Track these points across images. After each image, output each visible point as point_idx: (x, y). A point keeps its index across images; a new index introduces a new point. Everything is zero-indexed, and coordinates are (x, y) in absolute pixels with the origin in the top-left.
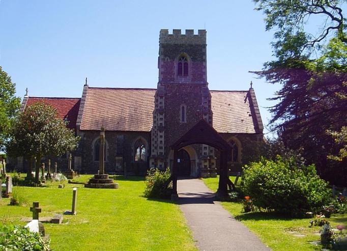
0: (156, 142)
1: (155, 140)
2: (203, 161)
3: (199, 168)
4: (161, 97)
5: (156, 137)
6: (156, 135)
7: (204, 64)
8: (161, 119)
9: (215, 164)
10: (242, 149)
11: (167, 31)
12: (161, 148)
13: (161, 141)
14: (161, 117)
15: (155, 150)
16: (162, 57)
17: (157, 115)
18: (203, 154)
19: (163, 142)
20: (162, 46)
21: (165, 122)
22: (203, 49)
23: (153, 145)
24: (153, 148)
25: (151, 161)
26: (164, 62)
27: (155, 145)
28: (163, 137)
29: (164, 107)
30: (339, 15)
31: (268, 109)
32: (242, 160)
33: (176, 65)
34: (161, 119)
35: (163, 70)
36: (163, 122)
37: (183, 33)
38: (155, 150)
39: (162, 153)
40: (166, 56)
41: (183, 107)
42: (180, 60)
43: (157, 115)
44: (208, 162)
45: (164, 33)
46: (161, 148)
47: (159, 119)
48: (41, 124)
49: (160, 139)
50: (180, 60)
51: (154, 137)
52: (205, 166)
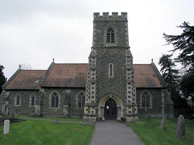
1: (89, 91)
2: (127, 108)
4: (94, 57)
8: (93, 74)
9: (137, 109)
14: (93, 72)
20: (95, 22)
21: (97, 77)
22: (125, 24)
23: (87, 95)
28: (95, 88)
33: (105, 35)
34: (93, 74)
35: (95, 39)
36: (95, 76)
37: (110, 14)
39: (94, 101)
40: (97, 29)
41: (111, 65)
42: (108, 32)
45: (96, 14)
46: (93, 97)
47: (91, 75)
50: (108, 32)
51: (88, 89)
52: (130, 112)
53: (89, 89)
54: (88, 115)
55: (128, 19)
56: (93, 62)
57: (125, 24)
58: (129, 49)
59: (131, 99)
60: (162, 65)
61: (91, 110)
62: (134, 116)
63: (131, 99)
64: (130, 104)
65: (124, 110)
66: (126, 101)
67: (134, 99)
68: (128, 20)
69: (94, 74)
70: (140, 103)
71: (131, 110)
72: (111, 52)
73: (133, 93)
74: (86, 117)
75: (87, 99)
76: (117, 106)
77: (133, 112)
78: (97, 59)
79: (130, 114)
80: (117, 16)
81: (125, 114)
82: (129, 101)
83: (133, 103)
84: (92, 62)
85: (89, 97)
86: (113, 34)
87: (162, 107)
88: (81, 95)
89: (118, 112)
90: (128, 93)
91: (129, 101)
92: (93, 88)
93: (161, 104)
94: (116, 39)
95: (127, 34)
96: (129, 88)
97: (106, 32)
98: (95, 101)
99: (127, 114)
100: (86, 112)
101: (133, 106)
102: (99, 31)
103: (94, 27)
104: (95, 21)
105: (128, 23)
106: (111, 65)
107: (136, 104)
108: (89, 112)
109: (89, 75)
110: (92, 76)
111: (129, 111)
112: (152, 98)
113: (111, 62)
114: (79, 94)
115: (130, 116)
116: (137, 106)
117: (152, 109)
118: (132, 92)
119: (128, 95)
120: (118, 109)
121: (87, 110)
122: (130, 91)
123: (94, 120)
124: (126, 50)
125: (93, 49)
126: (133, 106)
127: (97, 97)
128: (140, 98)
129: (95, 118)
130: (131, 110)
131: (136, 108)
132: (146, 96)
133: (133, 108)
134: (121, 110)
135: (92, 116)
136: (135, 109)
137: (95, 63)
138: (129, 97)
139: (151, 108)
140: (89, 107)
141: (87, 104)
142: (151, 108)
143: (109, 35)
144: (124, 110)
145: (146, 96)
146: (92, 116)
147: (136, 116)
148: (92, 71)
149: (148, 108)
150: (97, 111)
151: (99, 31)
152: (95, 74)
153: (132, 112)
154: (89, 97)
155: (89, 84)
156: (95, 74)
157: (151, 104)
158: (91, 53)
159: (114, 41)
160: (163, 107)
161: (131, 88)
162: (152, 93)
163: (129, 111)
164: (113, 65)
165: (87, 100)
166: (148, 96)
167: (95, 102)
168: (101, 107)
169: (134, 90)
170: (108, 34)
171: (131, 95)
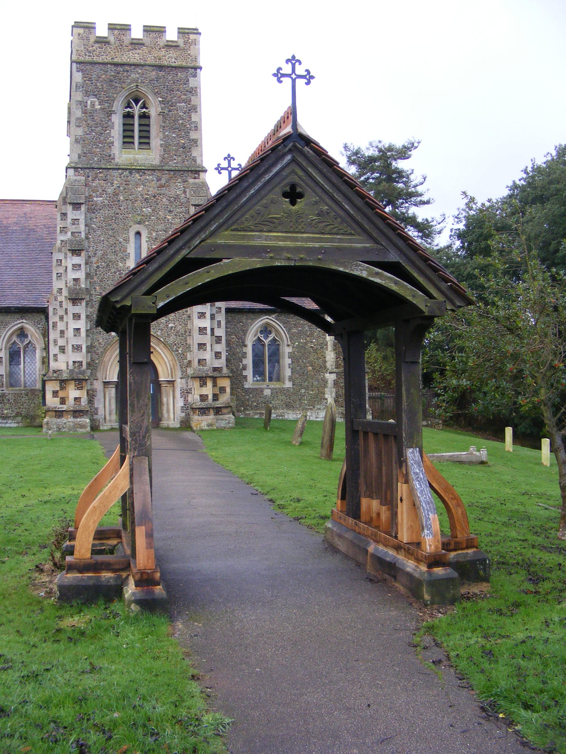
0: (62, 332)
1: (61, 326)
2: (197, 384)
3: (186, 400)
4: (76, 206)
5: (61, 318)
6: (61, 312)
7: (194, 118)
8: (76, 267)
9: (228, 390)
10: (245, 373)
11: (89, 27)
12: (77, 348)
13: (78, 330)
14: (77, 260)
15: (61, 357)
16: (79, 96)
17: (66, 258)
18: (195, 363)
19: (83, 333)
20: (79, 64)
21: (88, 275)
22: (191, 79)
23: (55, 341)
24: (54, 350)
25: (51, 387)
26: (85, 112)
27: (61, 342)
28: (83, 316)
29: (83, 235)
30: (109, 427)
31: (424, 198)
32: (290, 379)
33: (117, 120)
34: (76, 267)
35: (80, 132)
36: (81, 275)
37: (137, 33)
38: (61, 357)
39: (81, 363)
40: (87, 94)
41: (138, 233)
42: (129, 106)
43: (66, 258)
44: (210, 384)
45: (84, 28)
46: (77, 348)
47: (70, 267)
48: (433, 626)
49: (73, 325)
50: (129, 106)
51: (56, 319)
52: (203, 398)
53: (61, 318)
54: (59, 414)
55: (202, 62)
56: (75, 221)
57: (192, 82)
58: (202, 174)
59: (208, 355)
60: (358, 172)
61: (73, 393)
62: (218, 411)
63: (208, 355)
64: (207, 369)
65: (186, 392)
66: (190, 362)
67: (218, 355)
68: (201, 64)
69: (80, 266)
70: (245, 368)
71: (208, 390)
72: (137, 185)
73: (216, 334)
74: (55, 420)
75: (55, 355)
76: (160, 379)
77: (214, 400)
78: (89, 210)
79: (203, 405)
80: (162, 43)
81: (189, 409)
82: (201, 362)
83: (215, 369)
84: (69, 220)
85: (62, 350)
86: (145, 116)
87: (325, 382)
88: (18, 336)
89: (165, 400)
90: (195, 333)
91: (199, 361)
92: (77, 317)
93: (323, 368)
94: (156, 141)
95: (197, 120)
96: (199, 318)
97: (119, 107)
98: (84, 364)
99: (194, 406)
100: (52, 401)
101: (214, 379)
102: (93, 105)
103: (74, 87)
104: (77, 63)
105: (203, 75)
106: (138, 233)
107: (225, 371)
108: (63, 401)
109: (61, 270)
110: (72, 275)
111: (201, 396)
112: (291, 350)
113: (139, 223)
114: (12, 335)
115: (204, 411)
116: (229, 377)
117: (288, 389)
118: (212, 330)
119: (197, 338)
120: (163, 389)
121: (55, 394)
122: (205, 328)
123: (82, 426)
124: (191, 181)
125: (71, 171)
126: (216, 378)
127: (90, 349)
128: (246, 346)
129: (88, 421)
130: (208, 390)
131: (226, 383)
132: (267, 342)
133: (215, 385)
134: (174, 391)
135: (77, 413)
136: (222, 390)
137: (82, 227)
138: (202, 346)
139: (288, 384)
140: (63, 383)
141: (55, 372)
142: (288, 384)
143: (133, 117)
144: (186, 392)
145: (267, 342)
146: (77, 413)
147: (224, 411)
148: (69, 254)
149: (275, 385)
150: (91, 396)
151: (93, 105)
152: (83, 267)
153: (210, 397)
154: (62, 350)
155: (61, 302)
156: (83, 267)
157: (288, 372)
158: (66, 188)
159: (149, 143)
160: (330, 383)
161: (208, 315)
162: (289, 331)
163: (201, 396)
164: (147, 231)
165: (56, 360)
166: (274, 340)
167: (84, 366)
168: (106, 384)
169: (219, 322)
170: (128, 116)
171: (207, 339)
